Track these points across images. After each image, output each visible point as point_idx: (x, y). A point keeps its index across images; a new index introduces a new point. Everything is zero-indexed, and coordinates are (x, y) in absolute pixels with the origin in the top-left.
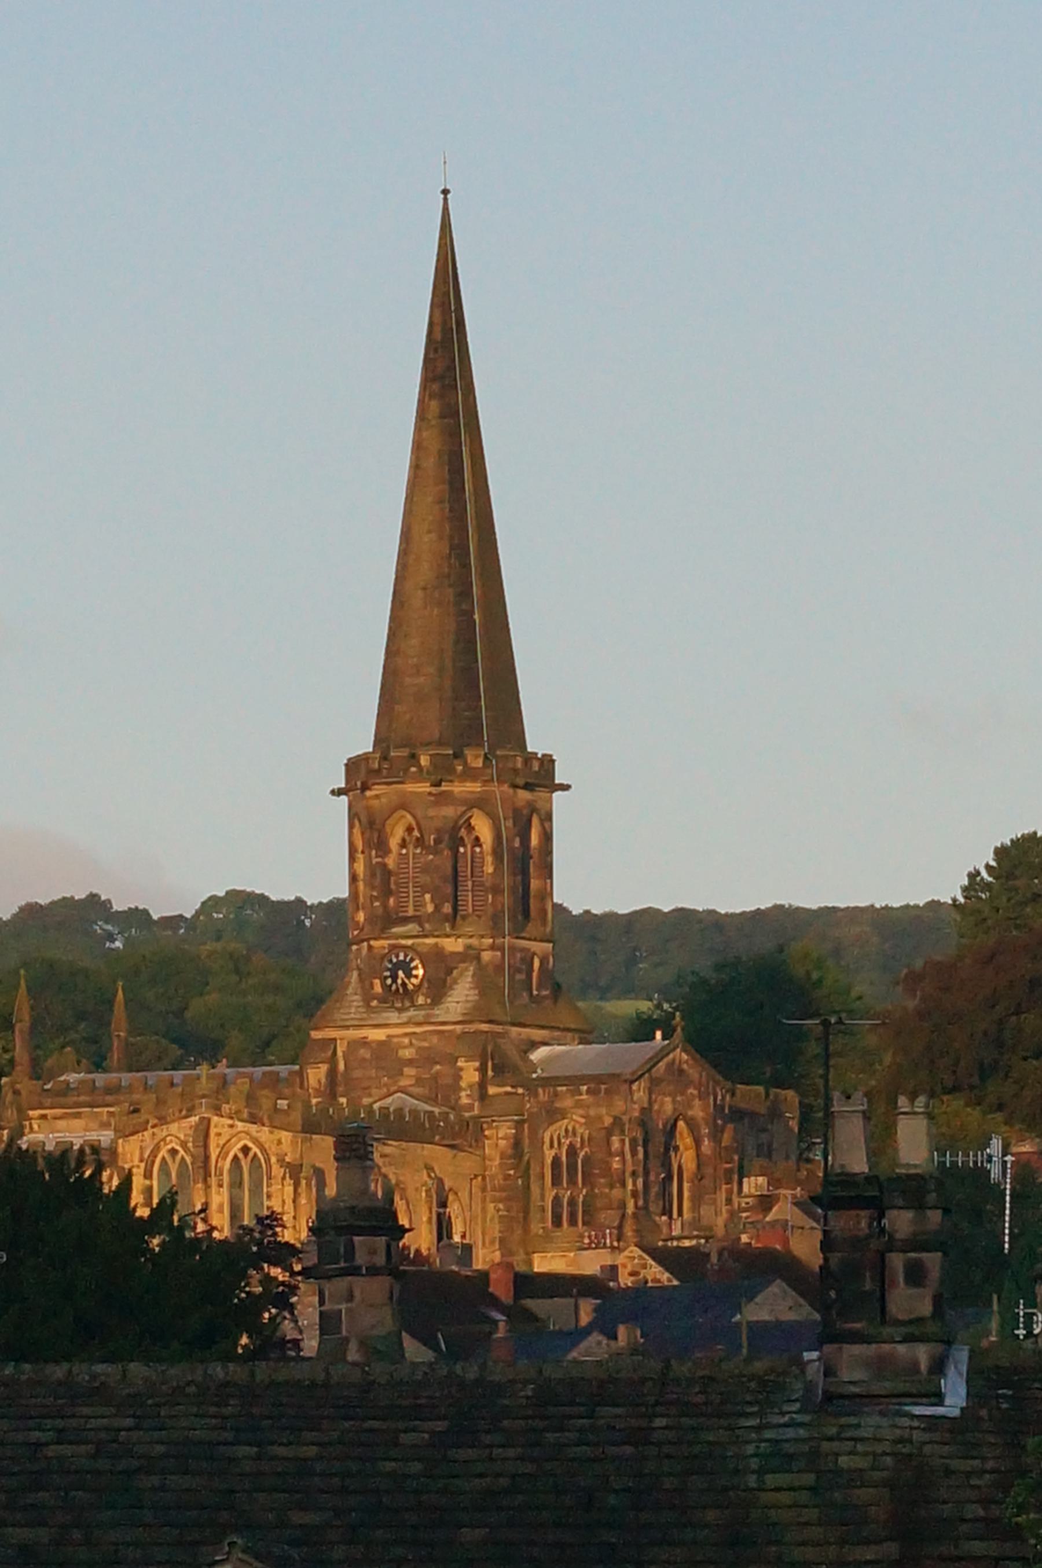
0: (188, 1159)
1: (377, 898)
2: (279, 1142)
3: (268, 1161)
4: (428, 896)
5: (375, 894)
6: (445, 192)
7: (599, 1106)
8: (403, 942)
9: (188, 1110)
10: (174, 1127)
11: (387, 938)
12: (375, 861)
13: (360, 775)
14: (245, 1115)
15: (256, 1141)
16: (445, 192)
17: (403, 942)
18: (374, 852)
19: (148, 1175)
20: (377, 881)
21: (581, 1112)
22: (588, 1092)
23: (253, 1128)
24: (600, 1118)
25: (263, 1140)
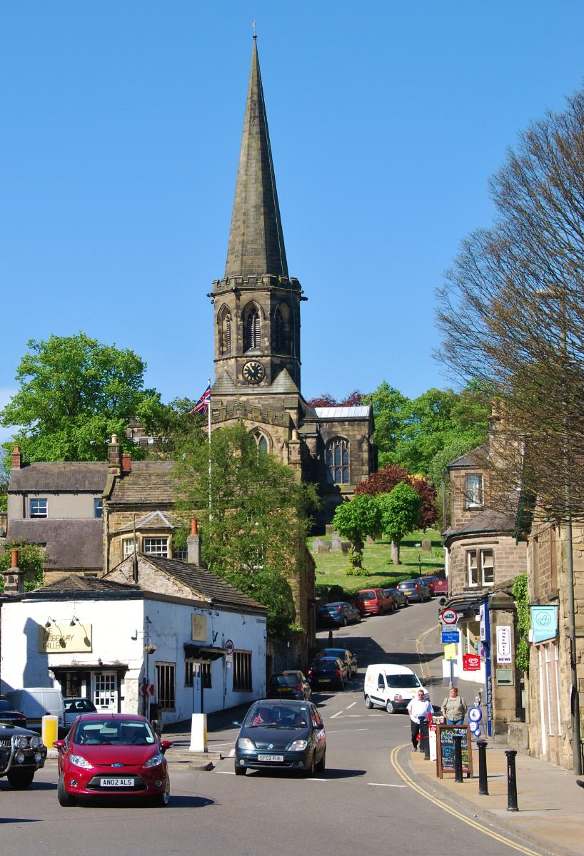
1: (240, 339)
2: (277, 432)
3: (271, 439)
4: (266, 339)
5: (239, 337)
7: (353, 430)
8: (254, 359)
9: (230, 416)
11: (246, 357)
12: (239, 323)
14: (260, 418)
17: (254, 359)
18: (239, 319)
20: (241, 332)
21: (345, 433)
22: (348, 425)
23: (263, 425)
24: (354, 436)
25: (268, 430)
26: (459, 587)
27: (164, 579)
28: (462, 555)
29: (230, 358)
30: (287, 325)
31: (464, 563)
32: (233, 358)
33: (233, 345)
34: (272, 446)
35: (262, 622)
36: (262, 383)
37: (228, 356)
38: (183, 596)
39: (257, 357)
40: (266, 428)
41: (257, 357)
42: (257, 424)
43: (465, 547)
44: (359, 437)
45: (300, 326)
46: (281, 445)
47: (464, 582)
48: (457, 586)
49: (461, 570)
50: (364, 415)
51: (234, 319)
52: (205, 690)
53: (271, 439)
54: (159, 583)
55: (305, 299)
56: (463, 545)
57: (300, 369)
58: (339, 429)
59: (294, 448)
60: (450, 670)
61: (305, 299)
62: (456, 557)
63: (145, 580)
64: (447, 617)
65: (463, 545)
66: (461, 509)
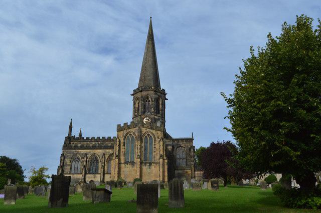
0: (134, 136)
3: (155, 137)
10: (132, 130)
13: (135, 92)
15: (151, 133)
19: (124, 139)
23: (151, 130)
33: (140, 111)
34: (155, 141)
40: (153, 132)
42: (148, 130)
44: (189, 146)
46: (159, 140)
53: (155, 137)
58: (181, 143)
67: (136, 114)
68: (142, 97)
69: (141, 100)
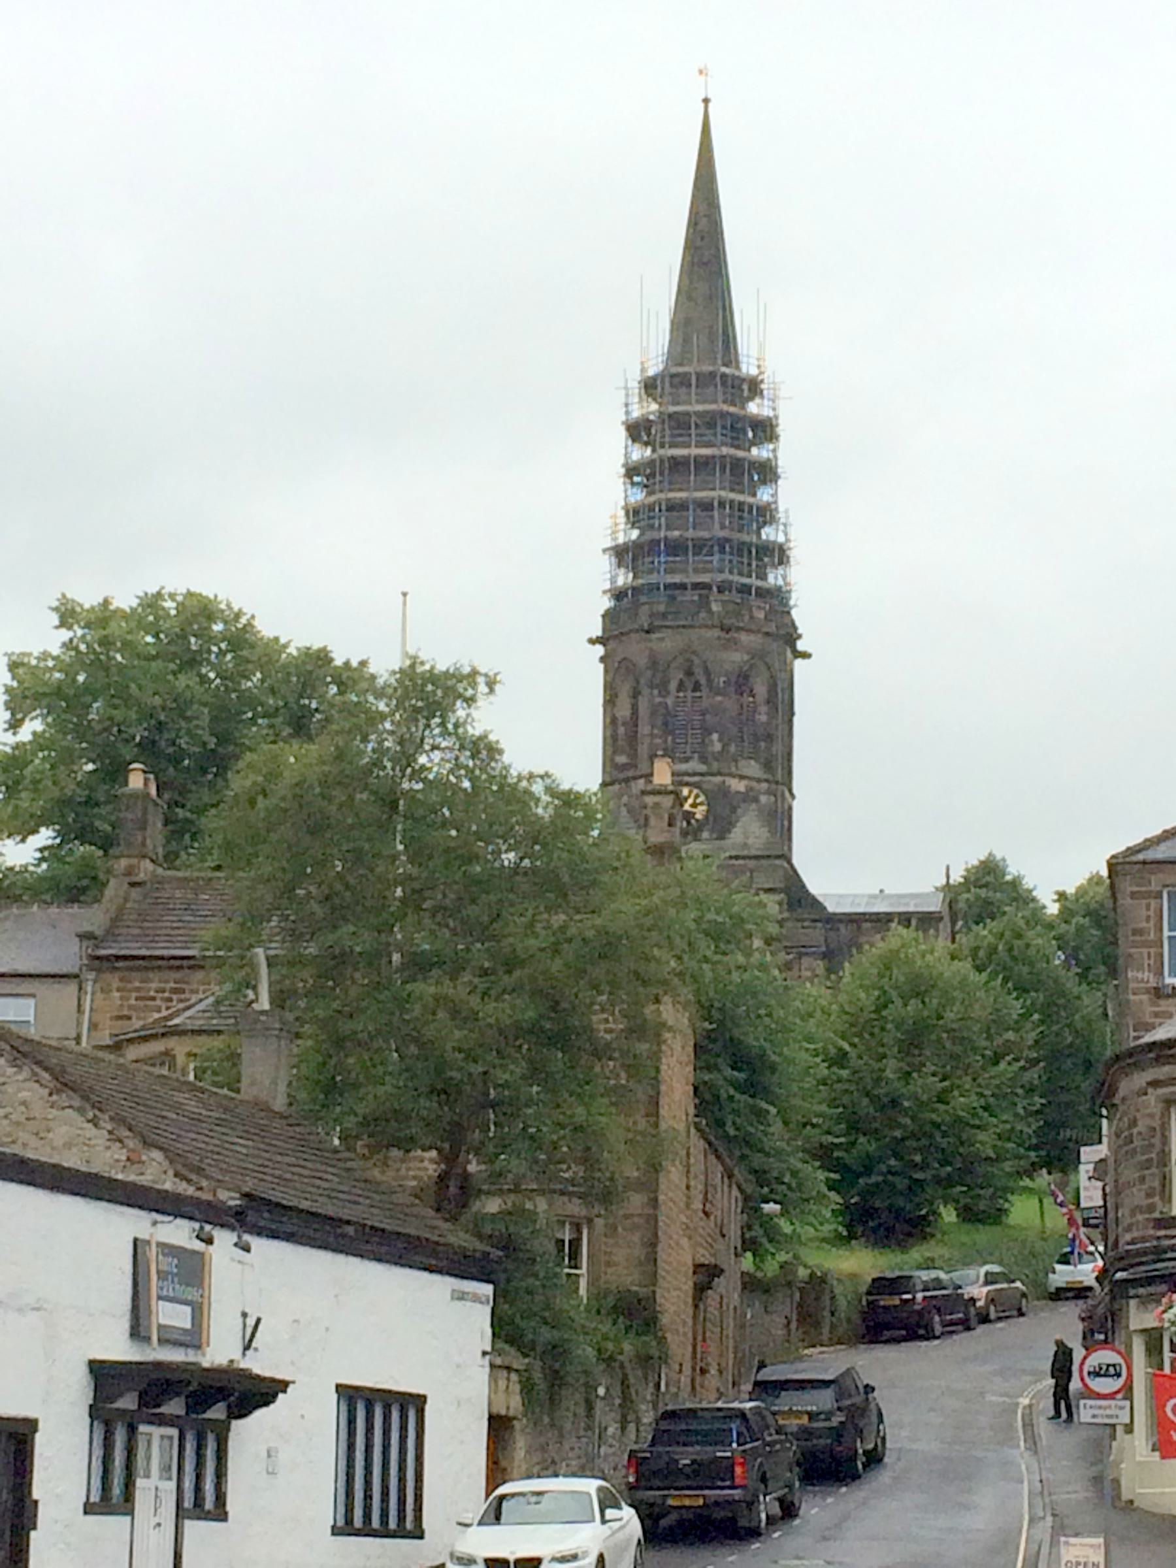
4: (715, 736)
6: (706, 101)
8: (687, 779)
12: (658, 700)
16: (706, 101)
17: (687, 779)
18: (656, 692)
20: (659, 722)
26: (1140, 1217)
27: (80, 1120)
28: (1151, 1116)
29: (635, 778)
30: (763, 709)
31: (1157, 1141)
32: (641, 777)
35: (476, 1299)
36: (705, 835)
37: (630, 773)
38: (145, 1180)
39: (695, 774)
41: (695, 774)
43: (1161, 1091)
45: (793, 714)
47: (1157, 1199)
48: (1133, 1213)
49: (1148, 1164)
50: (932, 909)
51: (646, 691)
52: (192, 1527)
54: (60, 1134)
55: (806, 655)
56: (1155, 1084)
57: (790, 808)
59: (657, 805)
60: (32, 971)
61: (806, 655)
62: (1134, 1123)
63: (18, 1124)
64: (1096, 1374)
65: (1155, 1084)
66: (1147, 991)
67: (622, 759)
68: (654, 664)
69: (652, 686)
